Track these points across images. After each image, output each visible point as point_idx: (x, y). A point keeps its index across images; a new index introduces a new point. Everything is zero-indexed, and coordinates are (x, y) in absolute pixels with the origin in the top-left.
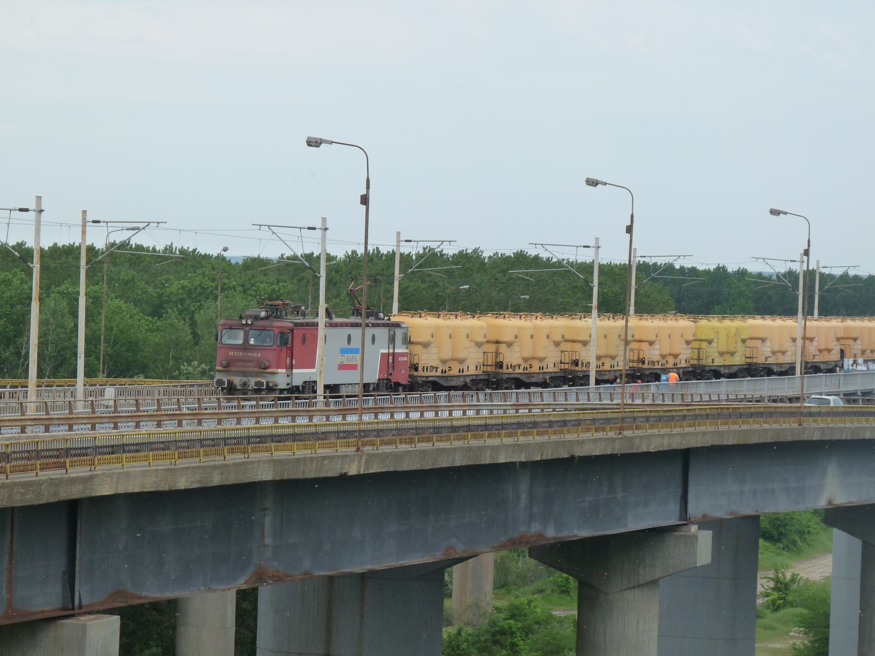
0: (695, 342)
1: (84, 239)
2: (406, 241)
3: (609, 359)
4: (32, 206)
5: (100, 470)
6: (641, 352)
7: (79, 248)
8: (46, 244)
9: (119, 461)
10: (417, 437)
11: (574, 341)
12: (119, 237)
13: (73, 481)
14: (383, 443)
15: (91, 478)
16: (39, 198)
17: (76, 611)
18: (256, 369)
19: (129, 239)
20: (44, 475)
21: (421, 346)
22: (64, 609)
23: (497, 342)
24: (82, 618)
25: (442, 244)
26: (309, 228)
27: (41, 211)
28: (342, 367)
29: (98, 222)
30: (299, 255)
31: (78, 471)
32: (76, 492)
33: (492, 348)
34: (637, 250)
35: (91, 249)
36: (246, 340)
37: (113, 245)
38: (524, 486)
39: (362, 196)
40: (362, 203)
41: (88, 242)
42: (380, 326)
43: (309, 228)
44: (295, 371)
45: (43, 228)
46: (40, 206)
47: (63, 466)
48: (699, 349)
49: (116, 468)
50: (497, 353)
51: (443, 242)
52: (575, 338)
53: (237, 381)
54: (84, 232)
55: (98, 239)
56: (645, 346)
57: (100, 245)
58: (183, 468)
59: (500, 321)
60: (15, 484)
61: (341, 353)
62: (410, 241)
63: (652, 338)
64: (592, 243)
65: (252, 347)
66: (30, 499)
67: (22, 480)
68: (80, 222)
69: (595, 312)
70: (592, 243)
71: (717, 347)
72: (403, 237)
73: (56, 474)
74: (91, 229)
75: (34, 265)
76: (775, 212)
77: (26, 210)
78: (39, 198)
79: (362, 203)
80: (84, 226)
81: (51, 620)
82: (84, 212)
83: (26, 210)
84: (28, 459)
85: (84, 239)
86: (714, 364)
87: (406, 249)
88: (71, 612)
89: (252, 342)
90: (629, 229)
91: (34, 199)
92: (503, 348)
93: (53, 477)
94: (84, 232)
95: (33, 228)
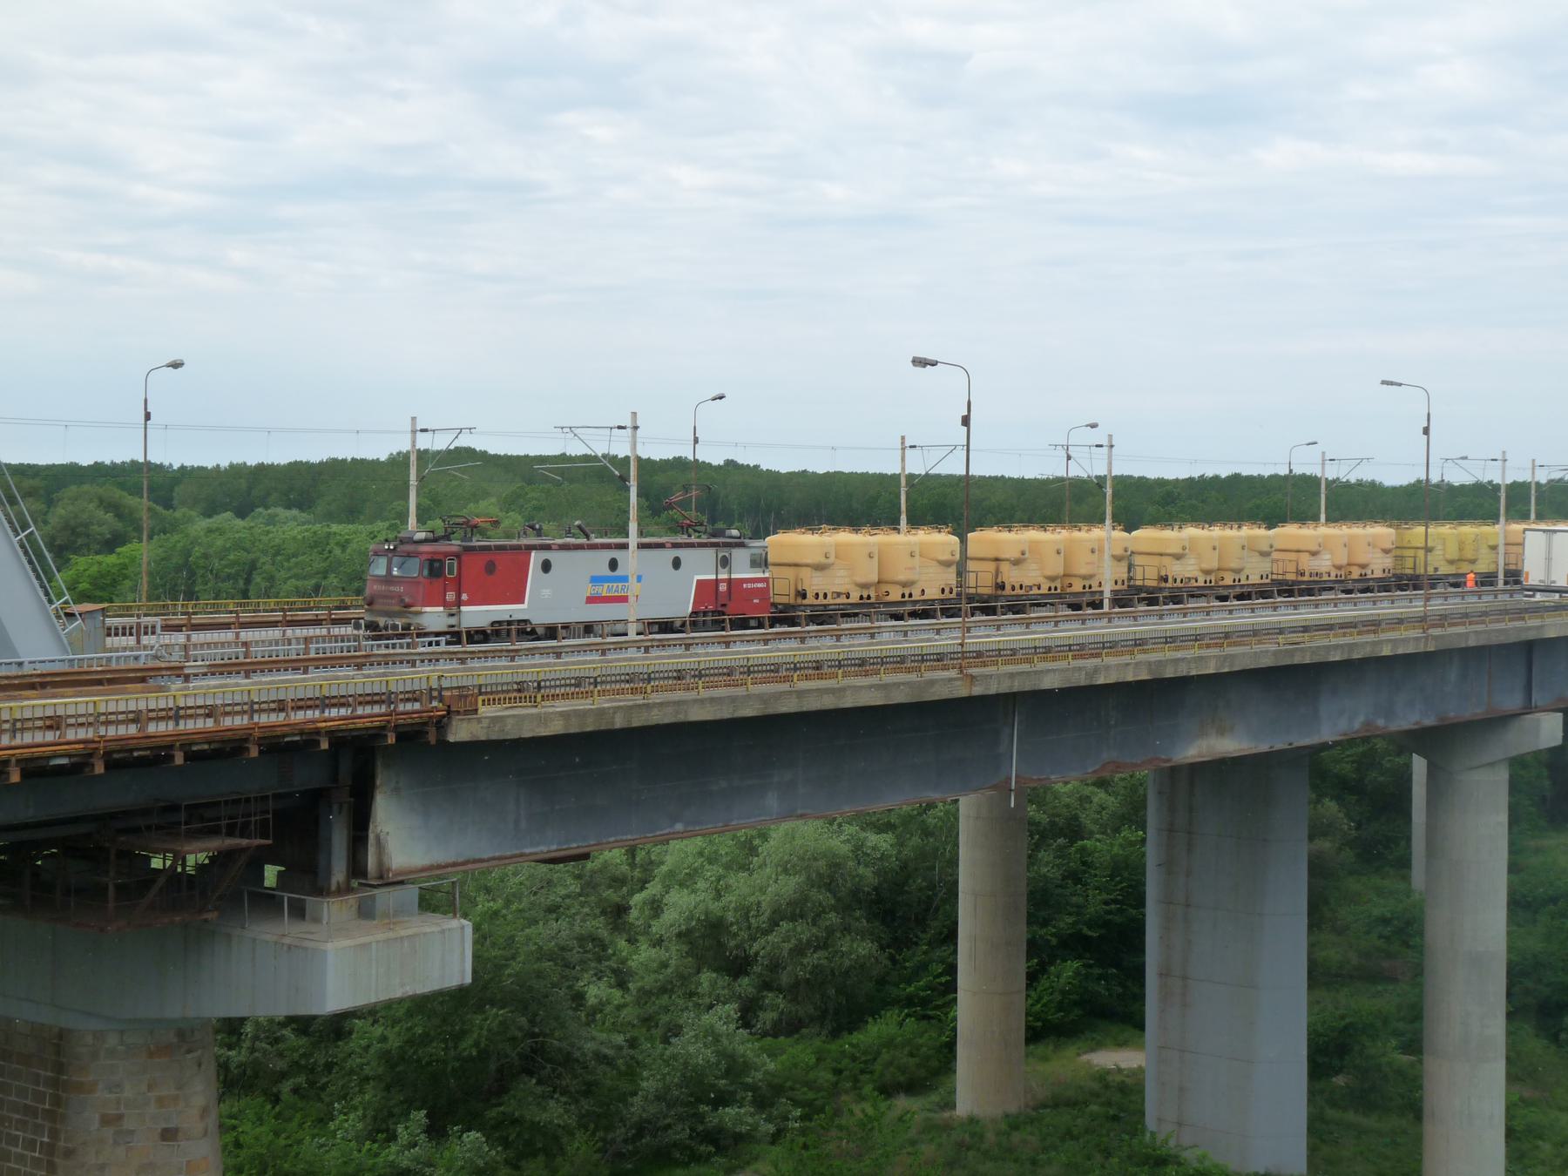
0: (1127, 558)
1: (1533, 477)
2: (1331, 460)
3: (1230, 573)
4: (1105, 443)
5: (1548, 621)
6: (1300, 564)
7: (1530, 483)
8: (1509, 481)
9: (1560, 615)
10: (1000, 659)
11: (1161, 555)
12: (1556, 475)
13: (1529, 629)
14: (1229, 645)
15: (1542, 626)
16: (1110, 436)
17: (1533, 710)
18: (397, 608)
19: (1564, 476)
20: (1511, 625)
21: (809, 569)
22: (1525, 708)
23: (997, 560)
24: (1537, 714)
25: (460, 432)
26: (1097, 446)
27: (1505, 460)
28: (591, 600)
29: (915, 447)
30: (600, 455)
31: (1533, 622)
32: (1531, 636)
33: (991, 566)
34: (418, 420)
35: (1538, 484)
36: (389, 570)
37: (1552, 481)
38: (1453, 674)
39: (1424, 428)
40: (1424, 434)
41: (1536, 480)
42: (598, 548)
43: (1097, 446)
44: (463, 608)
45: (1507, 472)
46: (636, 422)
47: (1523, 619)
48: (1415, 557)
49: (1558, 620)
50: (998, 571)
51: (956, 446)
52: (1163, 551)
53: (382, 621)
54: (1533, 473)
55: (1542, 477)
56: (1305, 557)
57: (1544, 481)
58: (640, 705)
59: (1076, 534)
60: (1492, 630)
61: (590, 583)
62: (1334, 460)
63: (1314, 548)
64: (1499, 457)
65: (397, 580)
66: (1503, 639)
67: (586, 707)
68: (1531, 466)
69: (1108, 521)
70: (1499, 457)
71: (1444, 555)
72: (1538, 463)
73: (1518, 624)
74: (1538, 470)
75: (632, 483)
76: (920, 362)
77: (1101, 446)
78: (1110, 436)
79: (1424, 434)
80: (1533, 469)
81: (1515, 715)
82: (903, 438)
83: (1101, 446)
84: (1501, 615)
85: (1533, 477)
86: (1438, 573)
87: (424, 442)
88: (1529, 711)
89: (395, 572)
90: (1426, 431)
91: (1501, 452)
92: (1005, 567)
93: (1081, 666)
94: (1533, 473)
95: (143, 430)
